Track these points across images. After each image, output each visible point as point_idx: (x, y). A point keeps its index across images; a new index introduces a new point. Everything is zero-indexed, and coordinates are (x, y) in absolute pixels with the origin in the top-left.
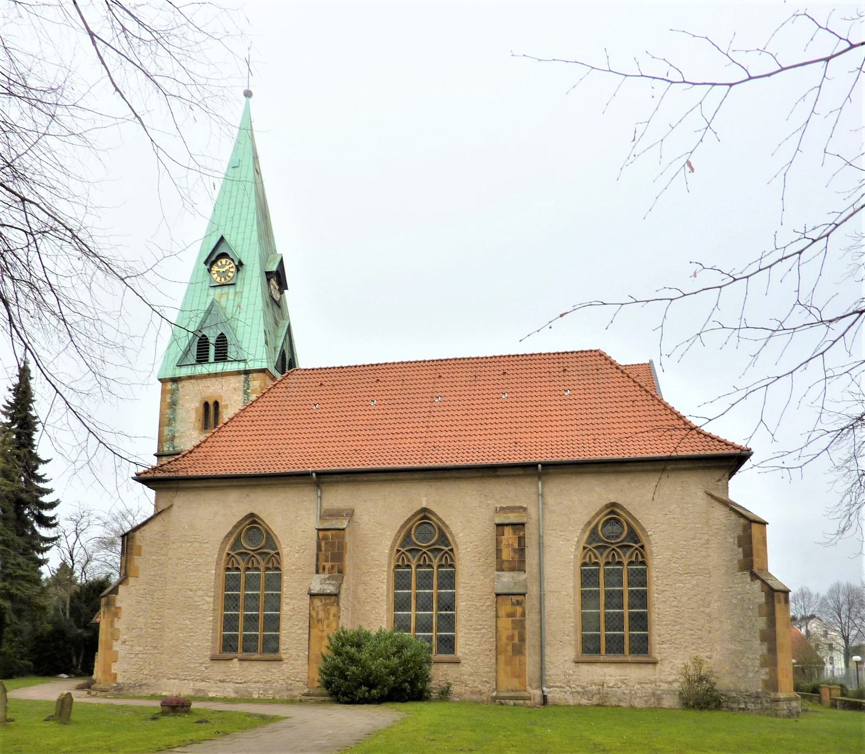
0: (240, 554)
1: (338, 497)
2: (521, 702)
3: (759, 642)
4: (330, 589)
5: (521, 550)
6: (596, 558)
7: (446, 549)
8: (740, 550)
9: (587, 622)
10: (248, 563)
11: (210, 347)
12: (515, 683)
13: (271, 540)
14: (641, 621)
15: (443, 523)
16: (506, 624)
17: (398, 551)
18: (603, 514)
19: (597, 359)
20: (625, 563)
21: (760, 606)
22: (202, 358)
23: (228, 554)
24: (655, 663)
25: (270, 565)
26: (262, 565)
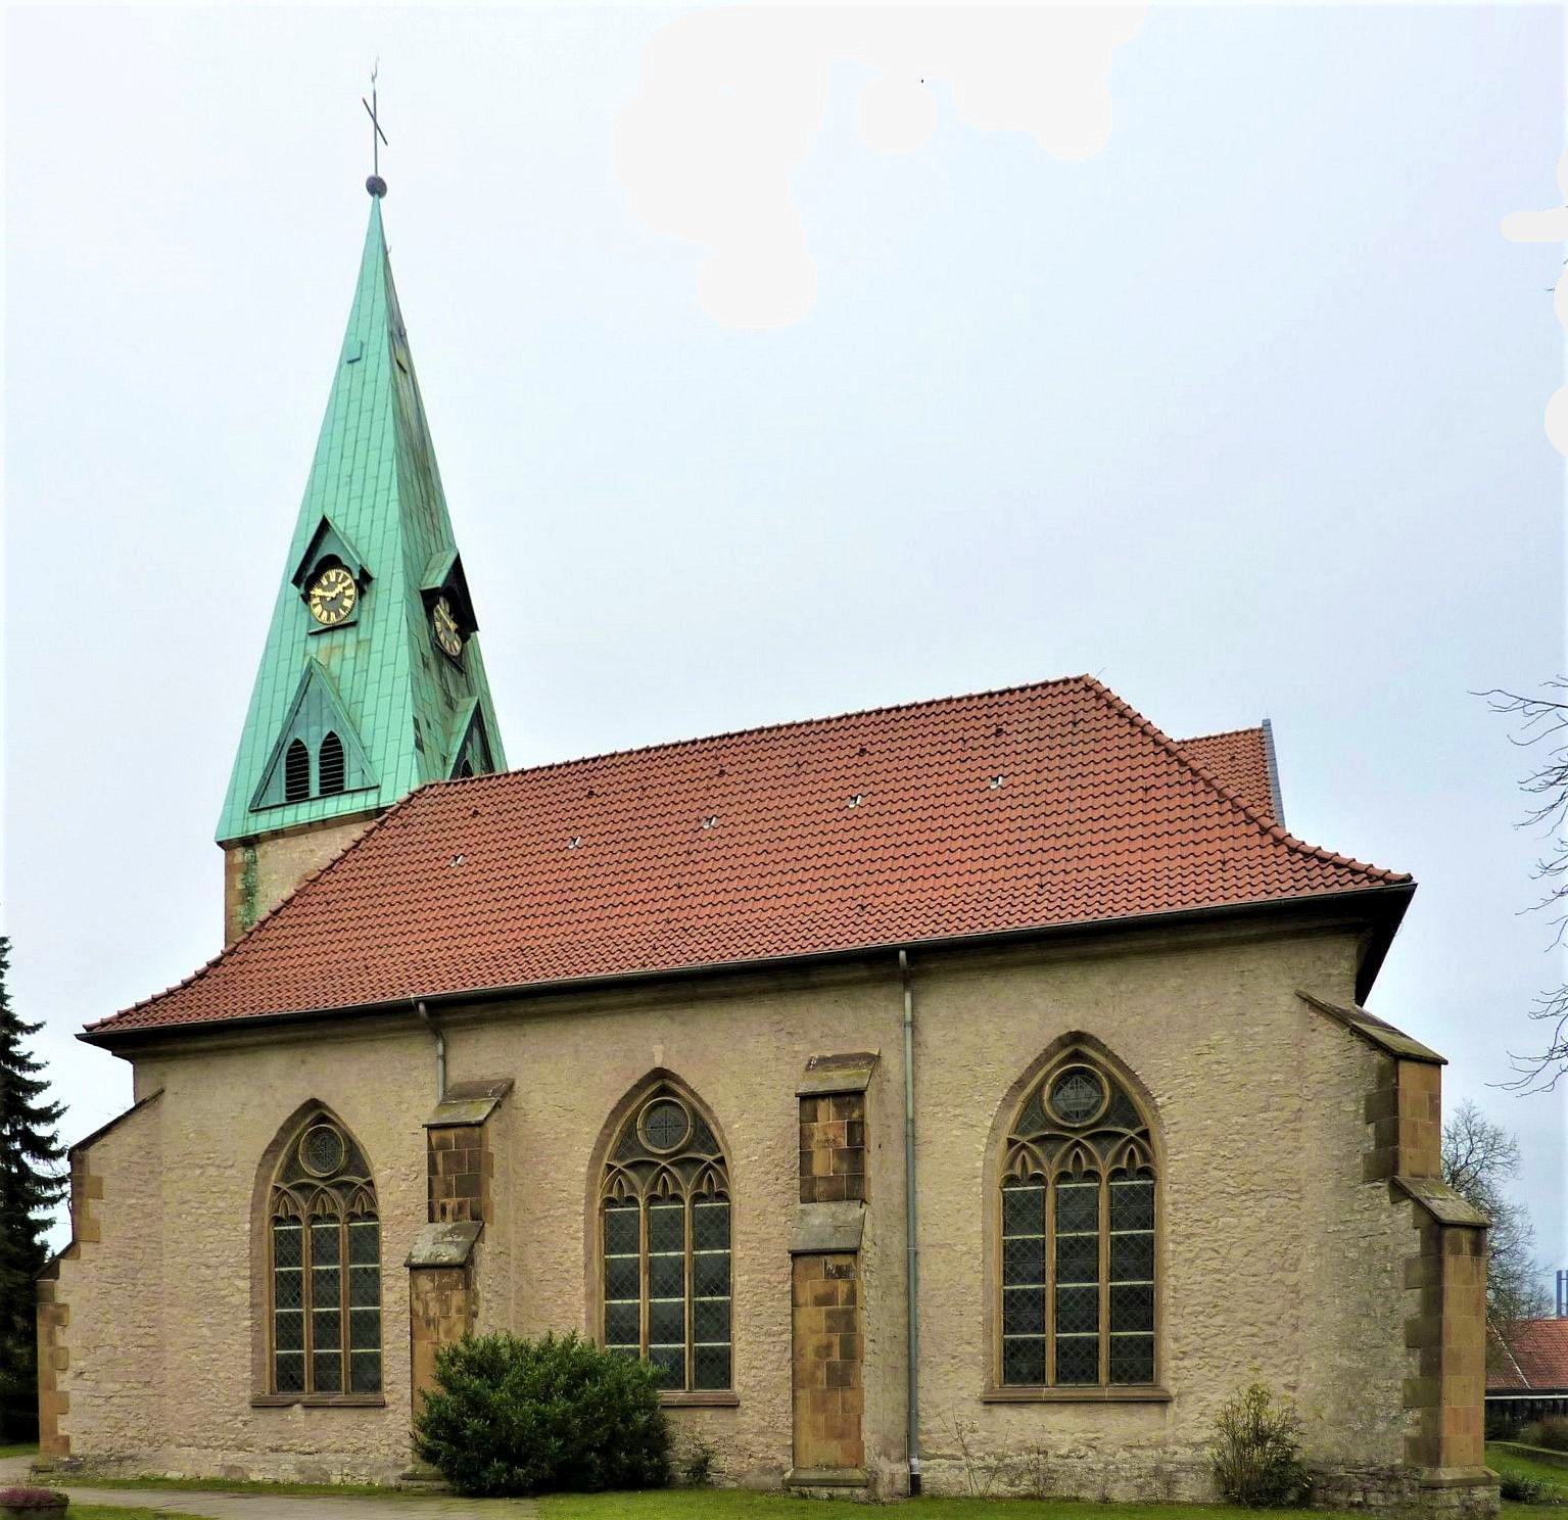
0: (301, 1188)
1: (482, 1056)
2: (845, 1491)
3: (1403, 1348)
4: (450, 1253)
5: (855, 1152)
8: (1370, 1129)
9: (1018, 1310)
11: (307, 765)
12: (833, 1451)
13: (356, 1160)
14: (1138, 1307)
15: (700, 1101)
16: (813, 1318)
17: (610, 1167)
18: (1054, 1061)
19: (1082, 705)
20: (1105, 1175)
22: (297, 792)
23: (277, 1189)
24: (1164, 1402)
25: (357, 1210)
26: (342, 1208)
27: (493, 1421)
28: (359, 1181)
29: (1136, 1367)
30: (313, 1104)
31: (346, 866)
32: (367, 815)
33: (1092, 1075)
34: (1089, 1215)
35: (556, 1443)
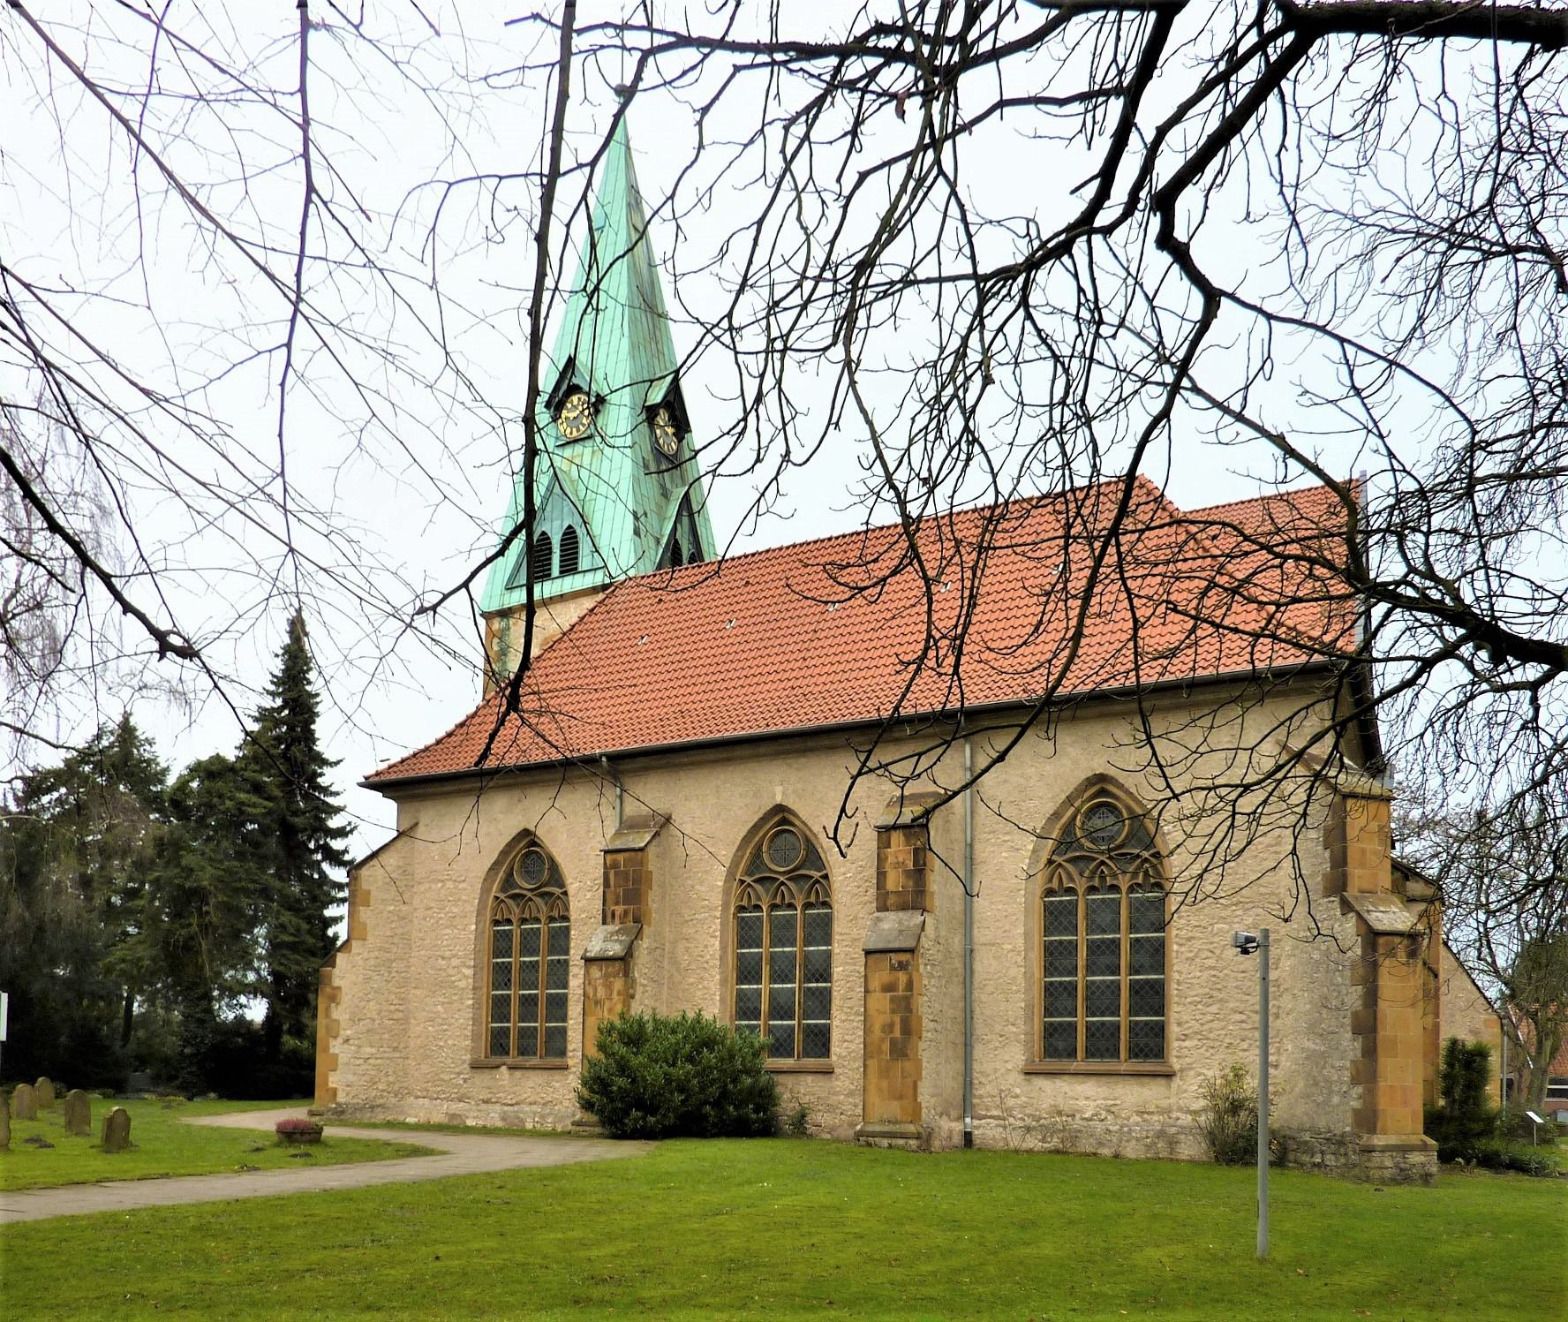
0: (514, 897)
1: (652, 794)
2: (901, 1142)
3: (1349, 1035)
4: (615, 949)
5: (919, 872)
6: (1072, 879)
7: (1146, 854)
8: (1327, 854)
9: (1056, 997)
10: (809, 895)
12: (894, 1109)
13: (556, 877)
14: (1152, 997)
16: (881, 1001)
18: (1086, 795)
20: (1124, 889)
24: (1169, 1076)
25: (555, 914)
27: (634, 1081)
28: (557, 891)
29: (1150, 1046)
30: (526, 833)
31: (563, 645)
32: (594, 590)
33: (1116, 808)
34: (1113, 921)
35: (678, 1097)
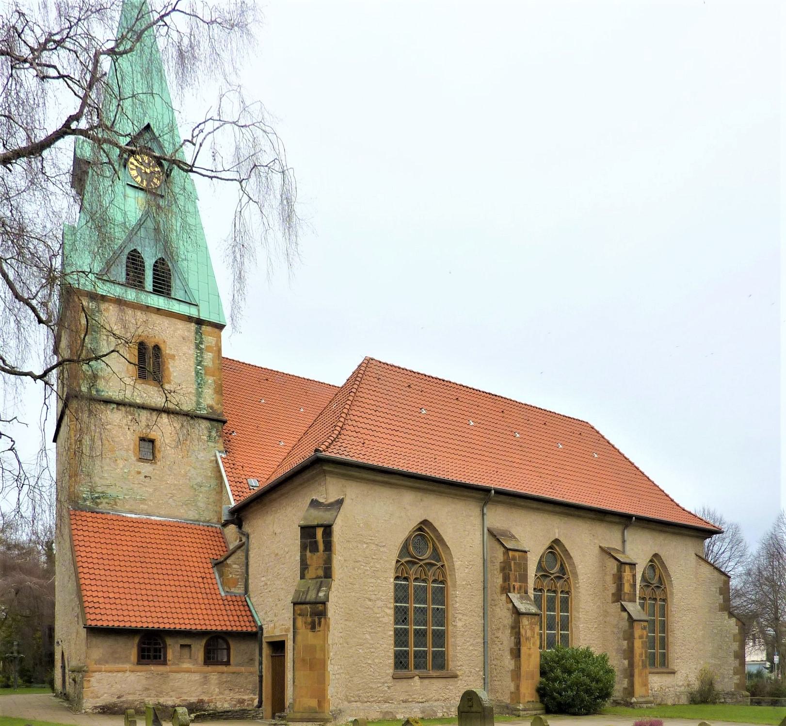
8: (721, 597)
21: (734, 636)
30: (425, 522)
